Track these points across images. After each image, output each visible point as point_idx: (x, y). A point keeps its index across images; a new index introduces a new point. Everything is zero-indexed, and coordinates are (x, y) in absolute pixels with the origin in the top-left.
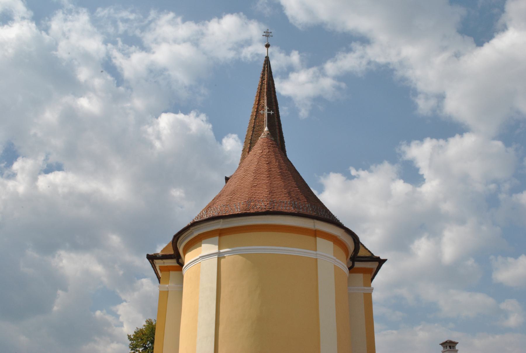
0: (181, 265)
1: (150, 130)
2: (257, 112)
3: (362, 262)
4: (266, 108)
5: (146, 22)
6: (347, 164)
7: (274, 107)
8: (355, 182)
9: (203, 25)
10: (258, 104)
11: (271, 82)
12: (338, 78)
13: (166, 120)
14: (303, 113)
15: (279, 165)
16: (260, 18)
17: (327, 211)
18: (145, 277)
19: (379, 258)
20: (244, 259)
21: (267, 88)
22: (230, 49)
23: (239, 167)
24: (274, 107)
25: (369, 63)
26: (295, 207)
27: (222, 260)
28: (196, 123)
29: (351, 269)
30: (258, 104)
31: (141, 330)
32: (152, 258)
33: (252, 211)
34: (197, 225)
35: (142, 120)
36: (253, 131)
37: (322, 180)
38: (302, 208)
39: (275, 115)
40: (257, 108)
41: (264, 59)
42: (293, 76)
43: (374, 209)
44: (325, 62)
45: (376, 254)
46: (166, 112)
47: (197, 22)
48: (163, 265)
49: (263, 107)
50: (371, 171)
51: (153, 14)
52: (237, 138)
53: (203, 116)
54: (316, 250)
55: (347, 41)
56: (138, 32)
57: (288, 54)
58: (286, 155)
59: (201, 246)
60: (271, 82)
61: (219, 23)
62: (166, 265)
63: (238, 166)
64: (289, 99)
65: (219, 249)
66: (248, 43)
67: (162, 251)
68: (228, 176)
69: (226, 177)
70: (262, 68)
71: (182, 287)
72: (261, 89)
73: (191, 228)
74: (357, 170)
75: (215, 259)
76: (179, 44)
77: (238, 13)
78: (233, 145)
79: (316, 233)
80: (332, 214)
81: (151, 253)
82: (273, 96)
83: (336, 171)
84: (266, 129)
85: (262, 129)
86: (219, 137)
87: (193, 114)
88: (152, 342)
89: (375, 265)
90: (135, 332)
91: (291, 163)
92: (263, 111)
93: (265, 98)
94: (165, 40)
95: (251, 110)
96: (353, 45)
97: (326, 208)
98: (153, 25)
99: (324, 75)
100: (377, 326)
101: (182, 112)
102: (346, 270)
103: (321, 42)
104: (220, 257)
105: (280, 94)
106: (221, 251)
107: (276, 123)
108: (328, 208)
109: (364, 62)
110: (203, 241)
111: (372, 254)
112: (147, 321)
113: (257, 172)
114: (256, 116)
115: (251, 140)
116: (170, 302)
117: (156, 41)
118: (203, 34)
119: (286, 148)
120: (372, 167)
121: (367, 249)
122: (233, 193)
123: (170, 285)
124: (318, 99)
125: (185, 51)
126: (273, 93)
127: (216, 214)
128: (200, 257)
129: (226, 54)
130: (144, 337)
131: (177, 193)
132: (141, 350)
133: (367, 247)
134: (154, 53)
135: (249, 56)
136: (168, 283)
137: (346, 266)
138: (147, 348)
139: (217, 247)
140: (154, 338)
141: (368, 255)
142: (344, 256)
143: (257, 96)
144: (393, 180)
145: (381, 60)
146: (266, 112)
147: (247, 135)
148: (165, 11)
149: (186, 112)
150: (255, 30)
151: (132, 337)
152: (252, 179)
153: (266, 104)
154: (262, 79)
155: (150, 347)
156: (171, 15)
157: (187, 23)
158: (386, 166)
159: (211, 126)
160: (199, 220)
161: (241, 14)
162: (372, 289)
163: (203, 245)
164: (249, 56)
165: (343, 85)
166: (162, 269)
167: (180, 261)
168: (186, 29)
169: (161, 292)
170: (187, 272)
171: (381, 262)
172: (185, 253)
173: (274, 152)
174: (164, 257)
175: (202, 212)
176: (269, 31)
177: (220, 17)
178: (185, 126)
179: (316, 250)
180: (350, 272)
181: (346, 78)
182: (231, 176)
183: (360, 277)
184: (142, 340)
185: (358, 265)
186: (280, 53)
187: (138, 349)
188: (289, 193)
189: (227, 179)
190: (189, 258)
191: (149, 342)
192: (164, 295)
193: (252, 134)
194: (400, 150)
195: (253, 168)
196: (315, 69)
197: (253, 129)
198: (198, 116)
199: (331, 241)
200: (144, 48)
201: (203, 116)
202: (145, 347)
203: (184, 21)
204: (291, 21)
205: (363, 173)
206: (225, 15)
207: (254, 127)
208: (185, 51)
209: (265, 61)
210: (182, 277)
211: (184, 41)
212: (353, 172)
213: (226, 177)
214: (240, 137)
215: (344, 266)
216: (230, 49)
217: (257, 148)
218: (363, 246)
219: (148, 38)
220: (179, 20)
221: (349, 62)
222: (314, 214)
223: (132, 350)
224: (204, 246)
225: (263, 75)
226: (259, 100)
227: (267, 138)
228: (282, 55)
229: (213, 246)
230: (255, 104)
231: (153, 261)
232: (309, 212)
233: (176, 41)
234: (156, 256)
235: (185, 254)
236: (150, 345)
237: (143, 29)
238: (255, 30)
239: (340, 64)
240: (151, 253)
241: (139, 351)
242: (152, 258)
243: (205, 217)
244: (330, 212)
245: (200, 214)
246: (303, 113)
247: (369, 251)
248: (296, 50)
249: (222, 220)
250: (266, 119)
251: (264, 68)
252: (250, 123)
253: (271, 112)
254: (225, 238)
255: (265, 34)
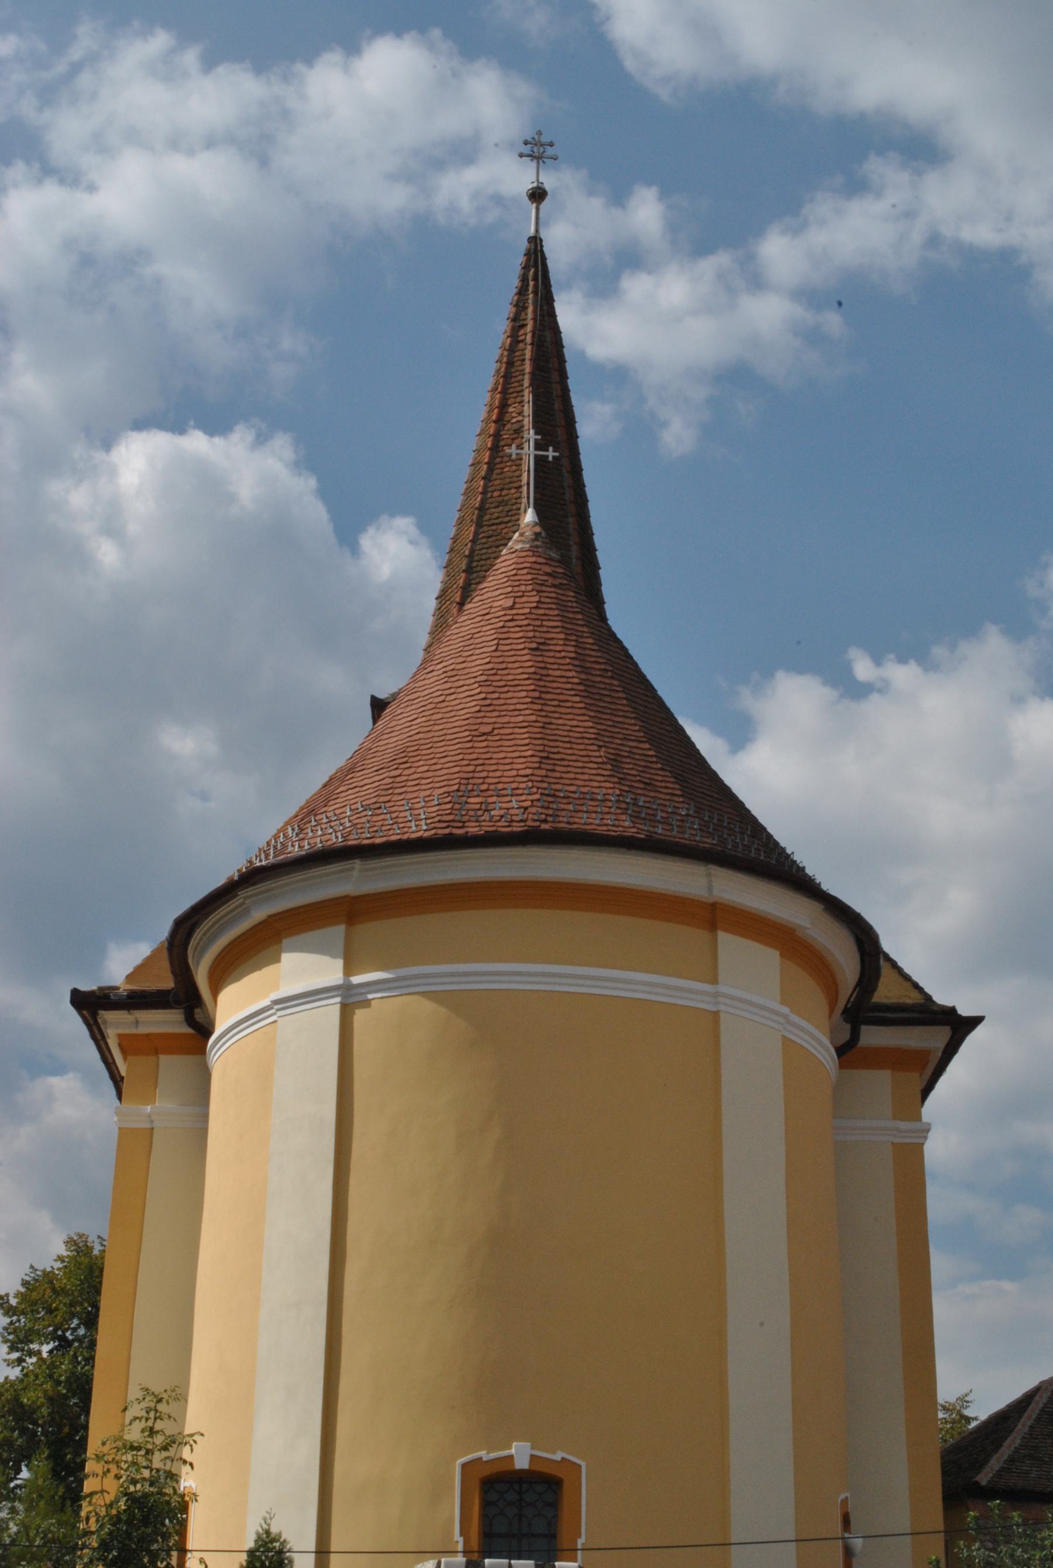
0: (203, 1030)
1: (79, 498)
2: (496, 449)
3: (889, 1026)
4: (531, 435)
5: (61, 68)
6: (849, 631)
7: (561, 433)
8: (875, 703)
9: (285, 79)
10: (500, 421)
11: (548, 334)
12: (809, 296)
13: (138, 461)
14: (678, 436)
15: (579, 657)
16: (510, 53)
17: (757, 830)
18: (59, 1069)
19: (953, 1010)
20: (442, 1010)
21: (534, 360)
22: (393, 177)
23: (425, 661)
24: (561, 433)
25: (934, 240)
26: (635, 817)
27: (360, 1016)
28: (253, 469)
29: (847, 1051)
30: (500, 421)
31: (48, 1277)
32: (90, 1004)
33: (473, 829)
34: (261, 881)
35: (44, 459)
36: (479, 524)
37: (746, 699)
38: (665, 822)
39: (565, 462)
40: (497, 436)
41: (524, 245)
42: (636, 286)
43: (946, 813)
44: (759, 232)
45: (942, 997)
46: (140, 425)
47: (260, 68)
48: (133, 1031)
49: (518, 431)
50: (928, 664)
51: (86, 36)
52: (414, 531)
53: (282, 444)
54: (714, 980)
55: (853, 148)
56: (27, 107)
57: (619, 198)
58: (603, 619)
59: (277, 960)
60: (548, 334)
61: (346, 69)
62: (143, 1030)
63: (420, 655)
64: (617, 376)
65: (348, 971)
66: (463, 151)
67: (129, 978)
68: (382, 695)
69: (374, 699)
70: (516, 282)
71: (205, 1117)
72: (510, 364)
73: (243, 894)
74: (878, 660)
75: (330, 1011)
76: (191, 152)
77: (423, 30)
78: (402, 559)
79: (714, 917)
80: (776, 844)
81: (87, 986)
82: (556, 390)
83: (799, 667)
84: (529, 516)
85: (514, 515)
86: (348, 532)
87: (240, 438)
88: (91, 1321)
89: (936, 1038)
90: (25, 1283)
91: (625, 650)
92: (520, 447)
93: (528, 396)
94: (134, 137)
95: (473, 443)
96: (876, 167)
97: (754, 821)
98: (85, 79)
99: (758, 282)
100: (941, 1265)
101: (199, 426)
102: (827, 1057)
103: (748, 153)
104: (351, 1001)
105: (582, 354)
106: (356, 980)
107: (569, 495)
108: (762, 820)
109: (917, 237)
110: (286, 942)
111: (928, 998)
112: (70, 1242)
113: (493, 680)
114: (491, 465)
115: (470, 556)
116: (157, 1167)
117: (101, 145)
118: (286, 115)
119: (604, 589)
120: (938, 651)
121: (907, 978)
122: (403, 758)
123: (161, 1109)
124: (734, 378)
125: (214, 179)
126: (555, 377)
127: (335, 840)
128: (276, 1002)
129: (378, 198)
130: (61, 1304)
131: (184, 742)
132: (45, 1349)
133: (907, 970)
134: (92, 188)
135: (466, 205)
136: (150, 1099)
137: (827, 1042)
138: (69, 1344)
139: (339, 963)
140: (96, 1307)
141: (912, 998)
142: (818, 1000)
143: (494, 390)
144: (1018, 700)
145: (983, 234)
146: (529, 452)
147: (455, 539)
148: (136, 24)
149: (216, 425)
150: (492, 101)
151: (13, 1302)
152: (472, 706)
153: (528, 422)
154: (517, 322)
155: (79, 1340)
156: (161, 41)
157: (221, 70)
158: (994, 647)
159: (313, 482)
160: (271, 860)
161: (436, 33)
162: (926, 1130)
163: (286, 957)
164: (466, 205)
165: (833, 321)
166: (131, 1045)
167: (198, 1014)
168: (218, 97)
169: (124, 1133)
170: (224, 1057)
171: (959, 1026)
172: (217, 985)
173: (561, 605)
174: (137, 1000)
175: (283, 829)
176: (545, 139)
177: (353, 49)
178: (210, 484)
179: (714, 980)
180: (842, 1066)
181: (844, 294)
182: (394, 696)
183: (880, 1082)
184: (50, 1311)
185: (873, 1037)
186: (591, 193)
187: (34, 1346)
188: (615, 762)
189: (378, 706)
190: (232, 1005)
191: (75, 1322)
192: (135, 1146)
193: (476, 534)
194: (1041, 584)
195: (478, 664)
196: (722, 259)
197: (480, 517)
198: (261, 440)
199: (775, 947)
200: (49, 170)
201: (282, 444)
202: (63, 1339)
203: (209, 63)
204: (630, 64)
205: (902, 675)
206: (370, 39)
207: (482, 509)
208: (214, 179)
209: (528, 254)
210: (206, 1075)
211: (210, 142)
212: (863, 669)
213: (374, 699)
214: (424, 528)
215: (818, 1043)
216: (393, 177)
217: (494, 591)
218: (894, 965)
219: (67, 130)
220: (191, 58)
221: (858, 230)
222: (709, 842)
223: (13, 1348)
224: (290, 960)
225: (520, 306)
226: (503, 406)
227: (533, 550)
228: (597, 204)
229: (325, 960)
230: (486, 421)
231: (94, 1015)
232: (692, 835)
233: (177, 142)
234: (106, 996)
235: (215, 991)
236: (82, 1331)
237: (48, 95)
238: (492, 101)
239: (818, 238)
240: (86, 986)
241: (39, 1352)
242: (90, 1004)
243: (295, 851)
244: (770, 836)
245: (276, 837)
246: (678, 436)
247: (916, 986)
248: (649, 184)
249: (357, 864)
250: (527, 476)
251: (524, 280)
252: (468, 493)
253: (551, 454)
254: (370, 930)
255: (527, 149)
